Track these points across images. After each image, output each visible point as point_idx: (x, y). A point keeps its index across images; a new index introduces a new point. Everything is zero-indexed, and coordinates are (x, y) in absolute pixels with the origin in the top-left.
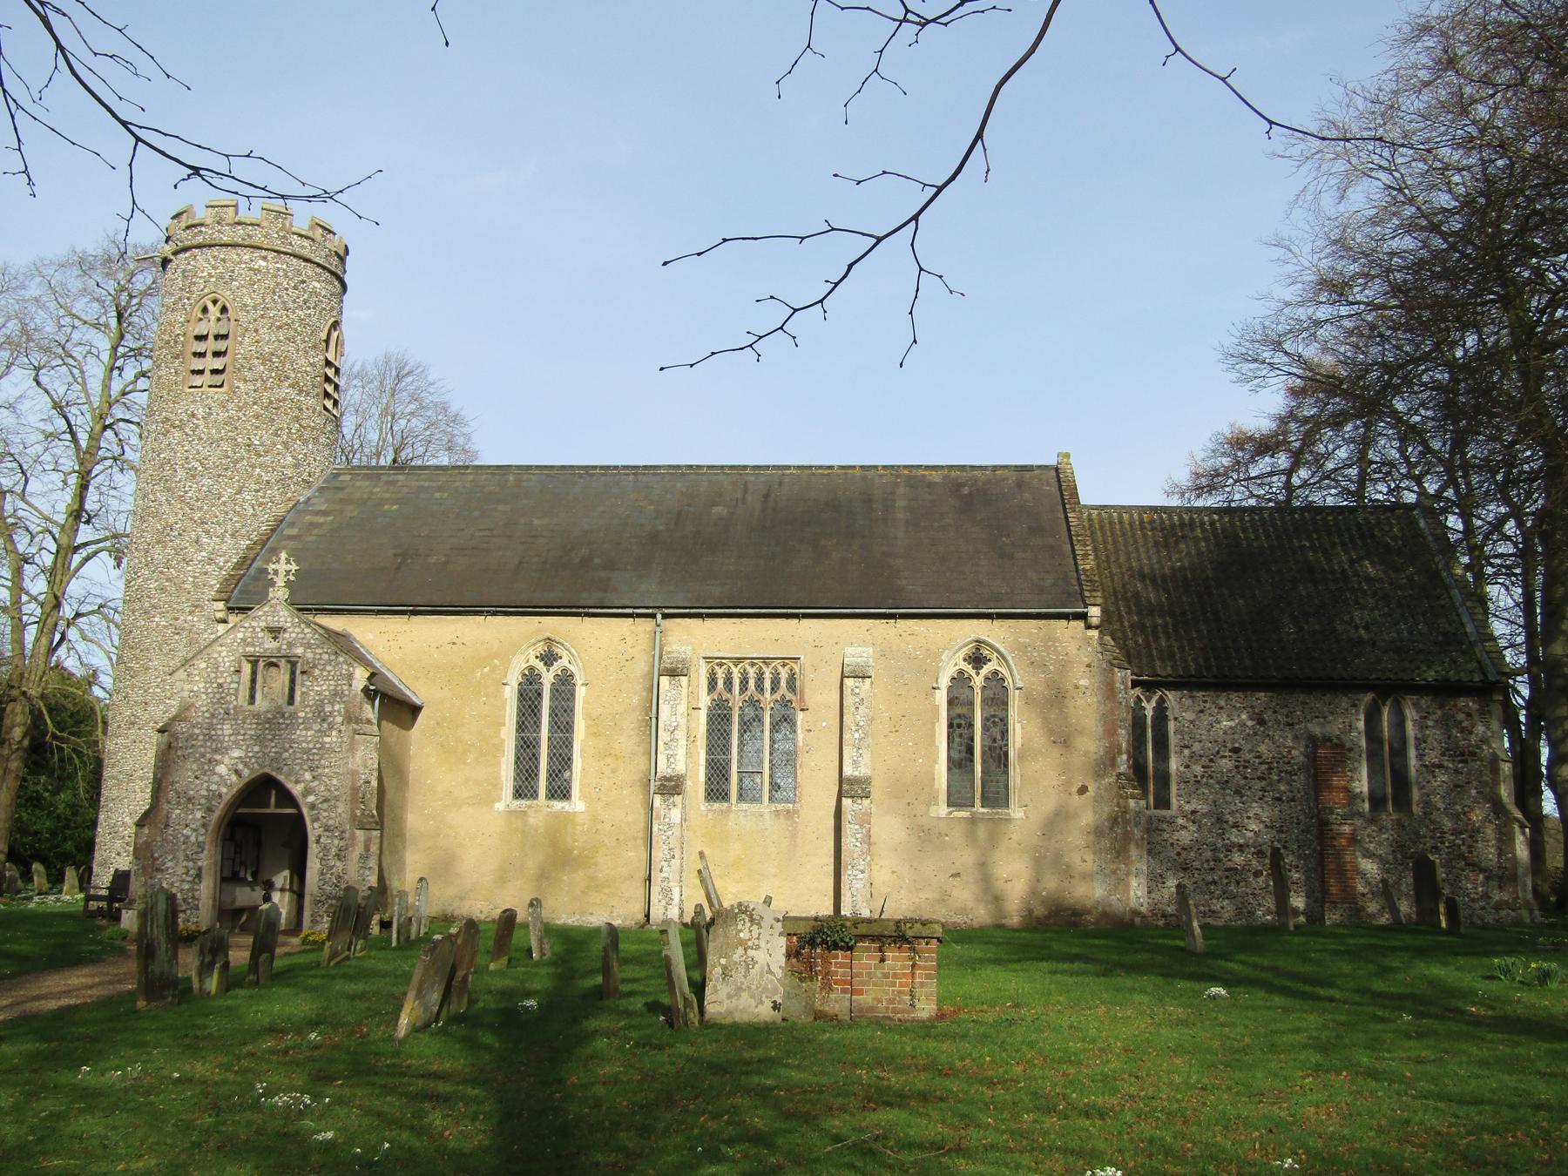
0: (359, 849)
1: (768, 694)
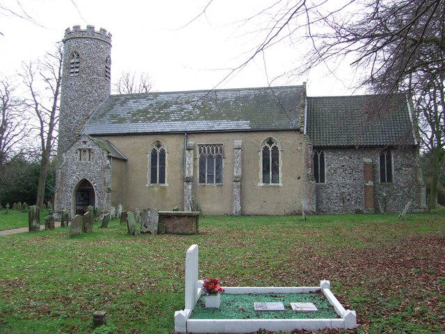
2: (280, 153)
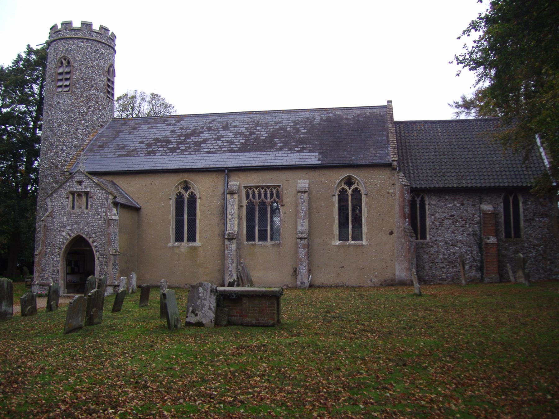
0: (112, 262)
1: (268, 200)
2: (364, 198)
